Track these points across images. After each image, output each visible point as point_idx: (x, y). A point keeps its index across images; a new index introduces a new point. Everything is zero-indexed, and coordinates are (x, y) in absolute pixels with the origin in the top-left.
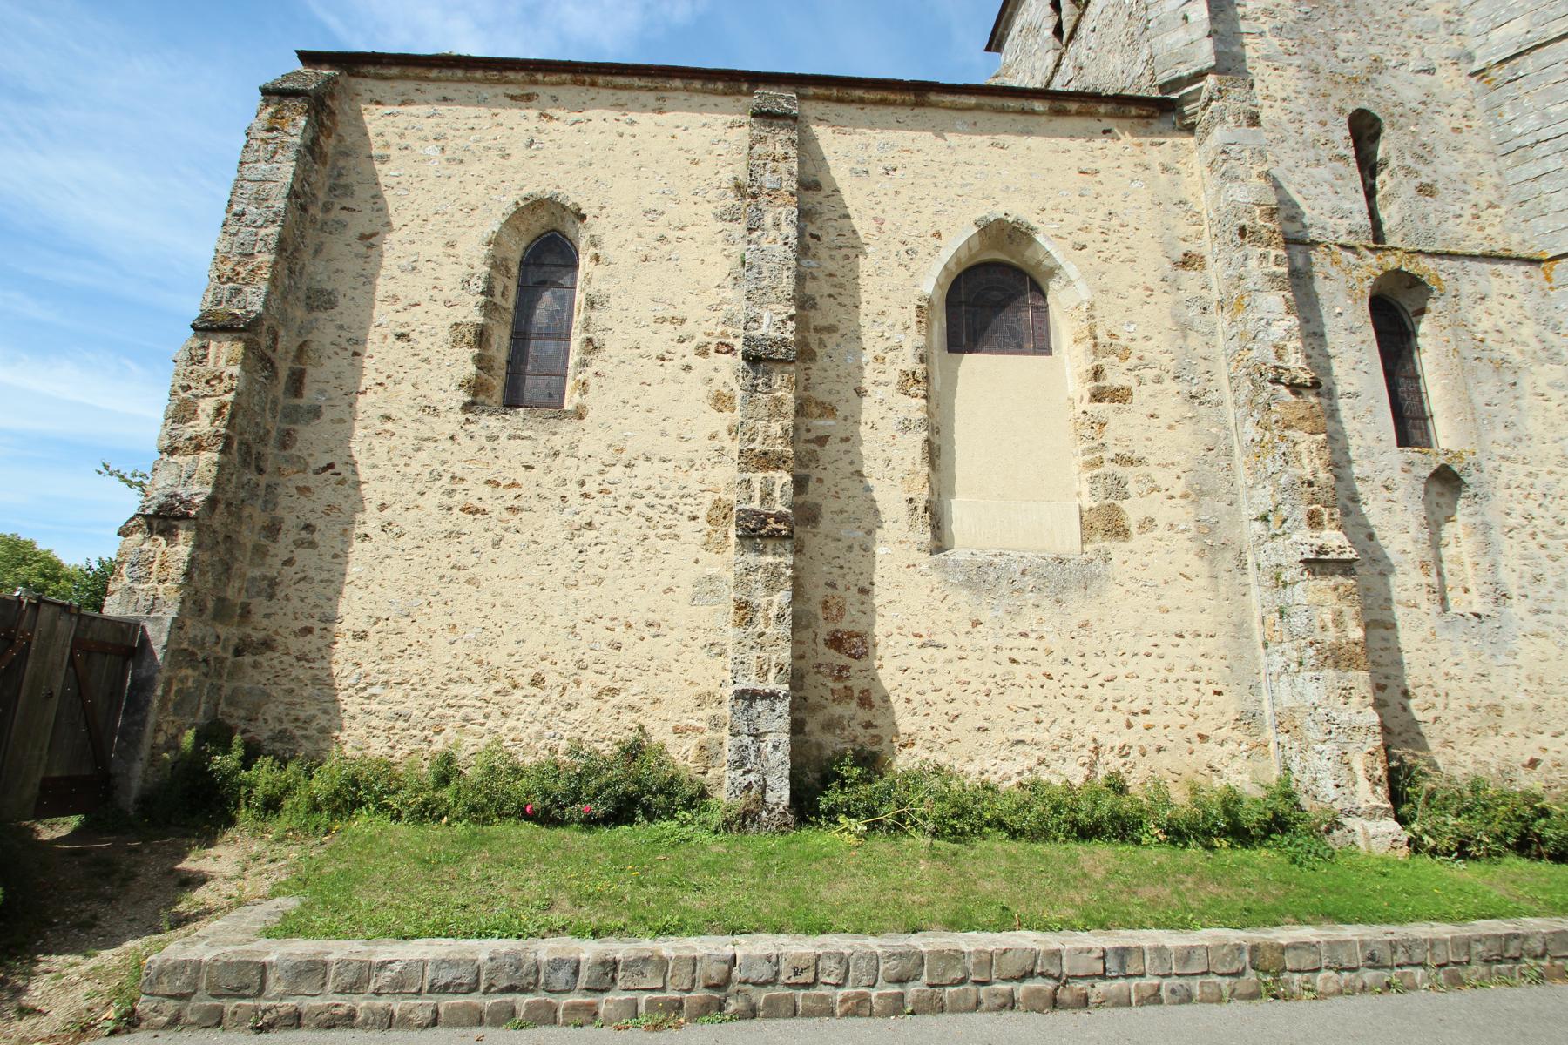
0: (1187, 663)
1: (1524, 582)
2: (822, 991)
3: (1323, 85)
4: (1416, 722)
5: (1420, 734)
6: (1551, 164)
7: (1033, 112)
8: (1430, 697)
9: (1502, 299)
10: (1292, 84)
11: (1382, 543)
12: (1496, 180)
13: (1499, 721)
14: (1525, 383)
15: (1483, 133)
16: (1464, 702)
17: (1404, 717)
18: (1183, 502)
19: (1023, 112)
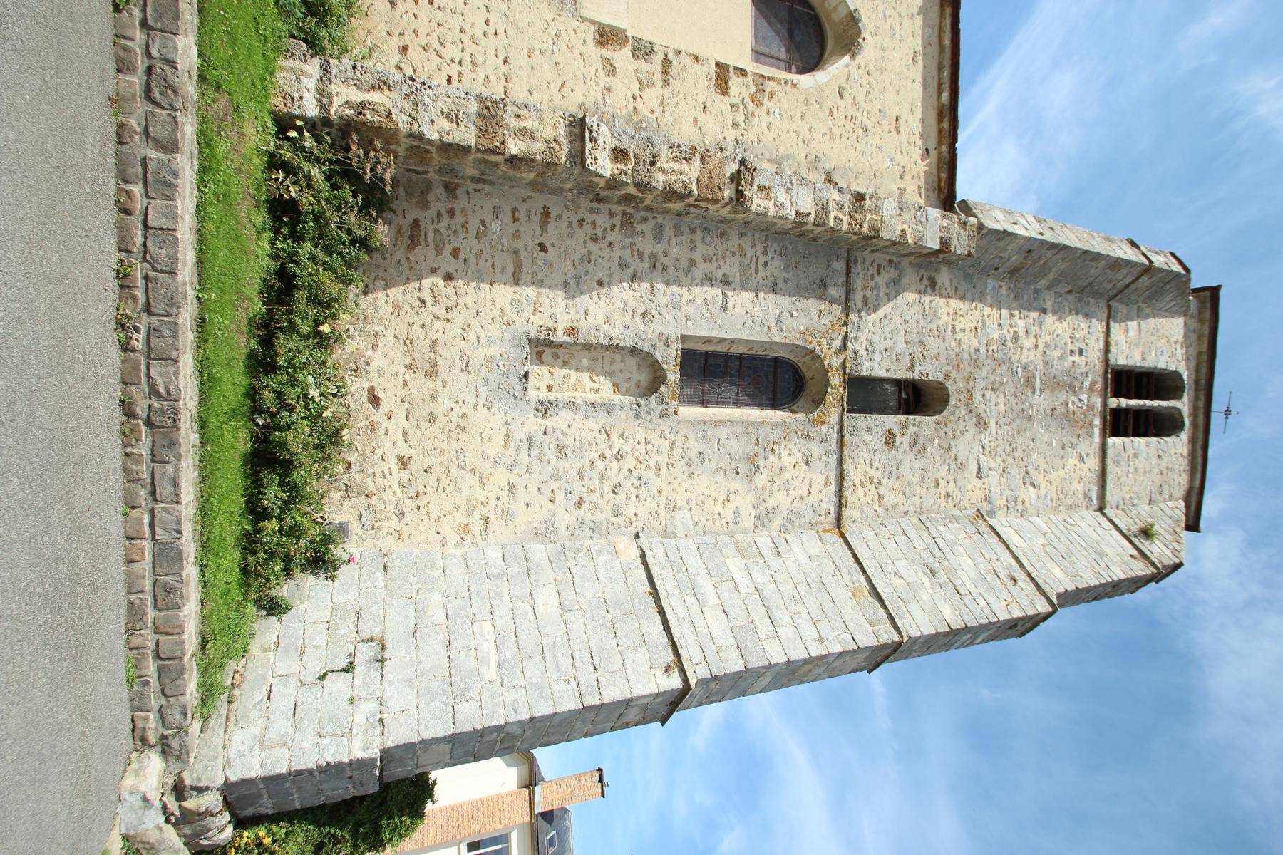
0: (479, 59)
1: (559, 434)
2: (139, 35)
3: (966, 368)
4: (420, 279)
5: (407, 281)
6: (917, 542)
7: (940, 93)
8: (445, 302)
9: (807, 481)
10: (966, 337)
11: (595, 294)
12: (901, 509)
13: (420, 372)
14: (738, 485)
15: (935, 507)
16: (440, 336)
17: (425, 268)
18: (630, 108)
19: (940, 85)
